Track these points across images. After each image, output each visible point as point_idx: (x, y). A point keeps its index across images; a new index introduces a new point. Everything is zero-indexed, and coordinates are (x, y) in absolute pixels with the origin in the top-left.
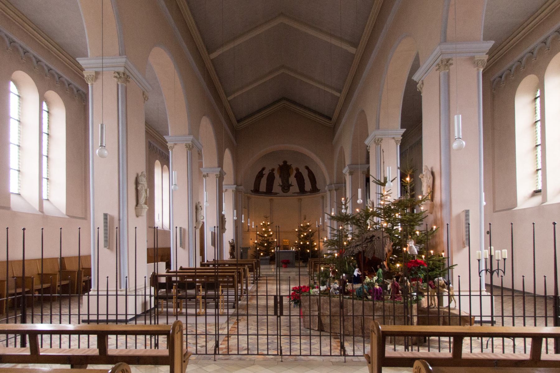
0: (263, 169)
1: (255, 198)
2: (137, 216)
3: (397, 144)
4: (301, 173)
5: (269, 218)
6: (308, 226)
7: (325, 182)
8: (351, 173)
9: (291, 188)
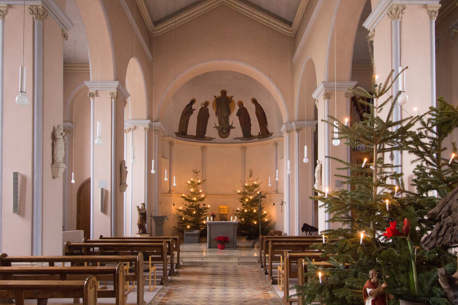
0: (193, 102)
1: (180, 143)
2: (54, 178)
3: (431, 17)
4: (245, 109)
5: (200, 174)
6: (256, 186)
7: (281, 122)
8: (328, 96)
9: (232, 130)
